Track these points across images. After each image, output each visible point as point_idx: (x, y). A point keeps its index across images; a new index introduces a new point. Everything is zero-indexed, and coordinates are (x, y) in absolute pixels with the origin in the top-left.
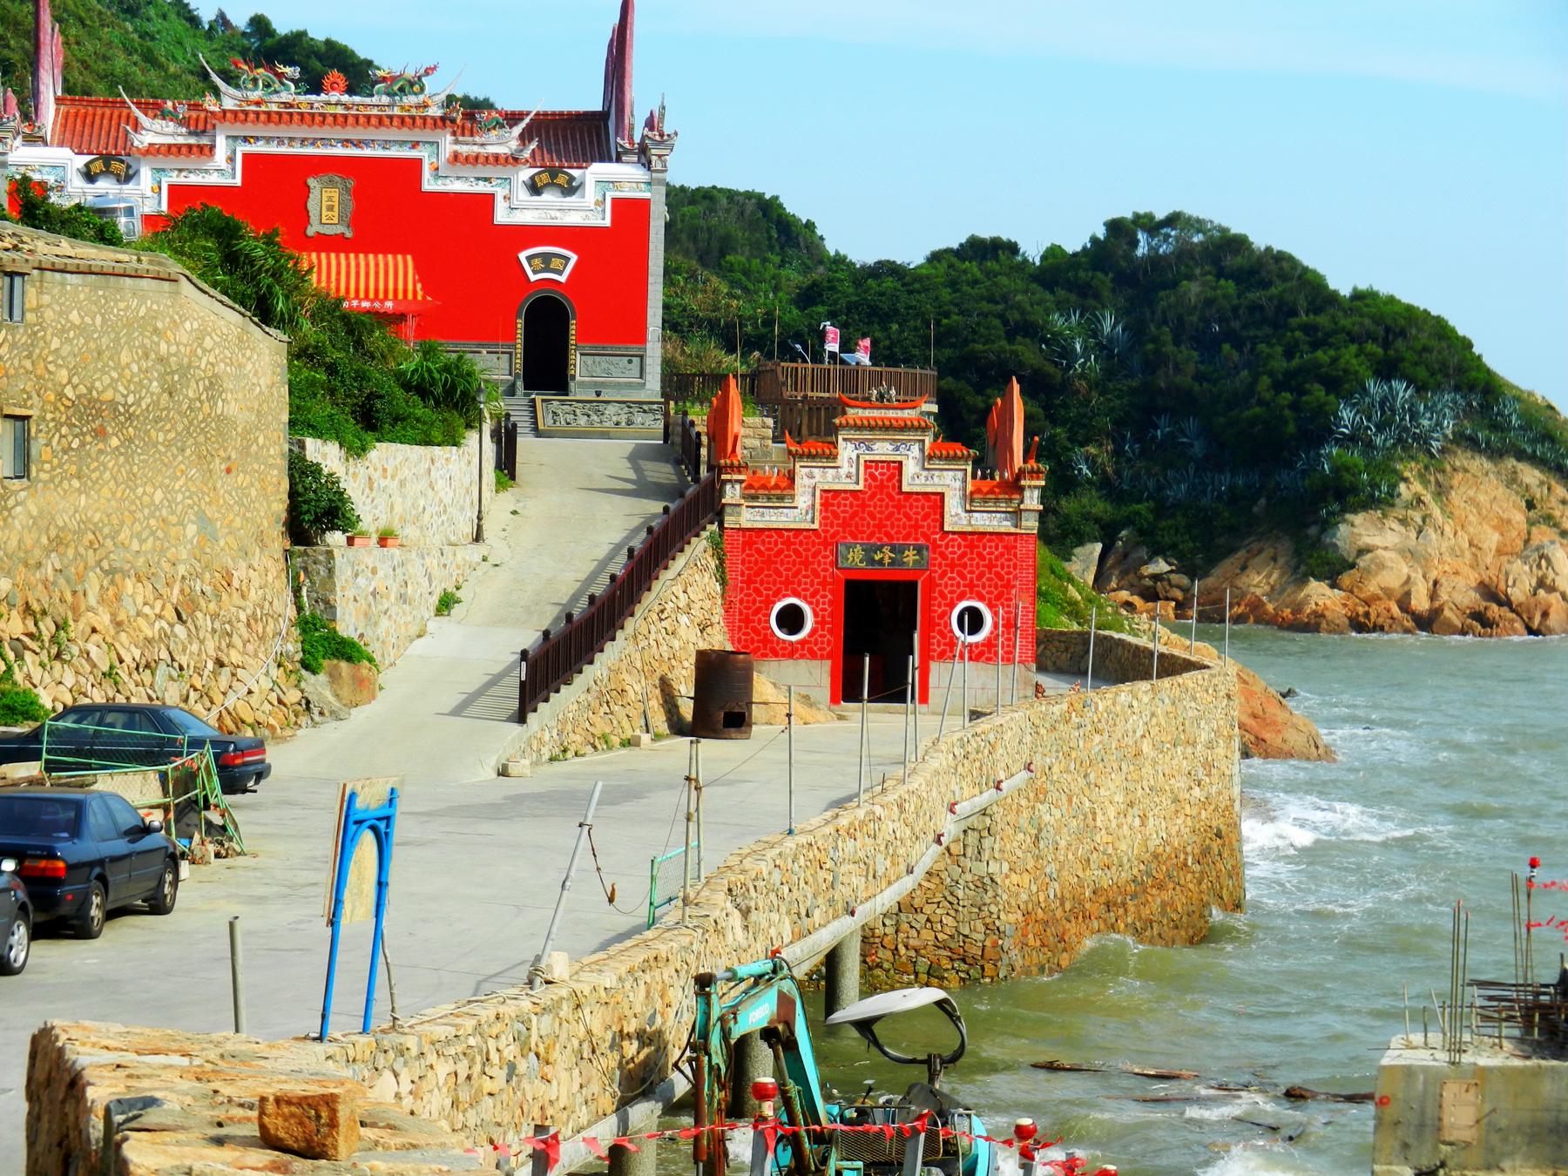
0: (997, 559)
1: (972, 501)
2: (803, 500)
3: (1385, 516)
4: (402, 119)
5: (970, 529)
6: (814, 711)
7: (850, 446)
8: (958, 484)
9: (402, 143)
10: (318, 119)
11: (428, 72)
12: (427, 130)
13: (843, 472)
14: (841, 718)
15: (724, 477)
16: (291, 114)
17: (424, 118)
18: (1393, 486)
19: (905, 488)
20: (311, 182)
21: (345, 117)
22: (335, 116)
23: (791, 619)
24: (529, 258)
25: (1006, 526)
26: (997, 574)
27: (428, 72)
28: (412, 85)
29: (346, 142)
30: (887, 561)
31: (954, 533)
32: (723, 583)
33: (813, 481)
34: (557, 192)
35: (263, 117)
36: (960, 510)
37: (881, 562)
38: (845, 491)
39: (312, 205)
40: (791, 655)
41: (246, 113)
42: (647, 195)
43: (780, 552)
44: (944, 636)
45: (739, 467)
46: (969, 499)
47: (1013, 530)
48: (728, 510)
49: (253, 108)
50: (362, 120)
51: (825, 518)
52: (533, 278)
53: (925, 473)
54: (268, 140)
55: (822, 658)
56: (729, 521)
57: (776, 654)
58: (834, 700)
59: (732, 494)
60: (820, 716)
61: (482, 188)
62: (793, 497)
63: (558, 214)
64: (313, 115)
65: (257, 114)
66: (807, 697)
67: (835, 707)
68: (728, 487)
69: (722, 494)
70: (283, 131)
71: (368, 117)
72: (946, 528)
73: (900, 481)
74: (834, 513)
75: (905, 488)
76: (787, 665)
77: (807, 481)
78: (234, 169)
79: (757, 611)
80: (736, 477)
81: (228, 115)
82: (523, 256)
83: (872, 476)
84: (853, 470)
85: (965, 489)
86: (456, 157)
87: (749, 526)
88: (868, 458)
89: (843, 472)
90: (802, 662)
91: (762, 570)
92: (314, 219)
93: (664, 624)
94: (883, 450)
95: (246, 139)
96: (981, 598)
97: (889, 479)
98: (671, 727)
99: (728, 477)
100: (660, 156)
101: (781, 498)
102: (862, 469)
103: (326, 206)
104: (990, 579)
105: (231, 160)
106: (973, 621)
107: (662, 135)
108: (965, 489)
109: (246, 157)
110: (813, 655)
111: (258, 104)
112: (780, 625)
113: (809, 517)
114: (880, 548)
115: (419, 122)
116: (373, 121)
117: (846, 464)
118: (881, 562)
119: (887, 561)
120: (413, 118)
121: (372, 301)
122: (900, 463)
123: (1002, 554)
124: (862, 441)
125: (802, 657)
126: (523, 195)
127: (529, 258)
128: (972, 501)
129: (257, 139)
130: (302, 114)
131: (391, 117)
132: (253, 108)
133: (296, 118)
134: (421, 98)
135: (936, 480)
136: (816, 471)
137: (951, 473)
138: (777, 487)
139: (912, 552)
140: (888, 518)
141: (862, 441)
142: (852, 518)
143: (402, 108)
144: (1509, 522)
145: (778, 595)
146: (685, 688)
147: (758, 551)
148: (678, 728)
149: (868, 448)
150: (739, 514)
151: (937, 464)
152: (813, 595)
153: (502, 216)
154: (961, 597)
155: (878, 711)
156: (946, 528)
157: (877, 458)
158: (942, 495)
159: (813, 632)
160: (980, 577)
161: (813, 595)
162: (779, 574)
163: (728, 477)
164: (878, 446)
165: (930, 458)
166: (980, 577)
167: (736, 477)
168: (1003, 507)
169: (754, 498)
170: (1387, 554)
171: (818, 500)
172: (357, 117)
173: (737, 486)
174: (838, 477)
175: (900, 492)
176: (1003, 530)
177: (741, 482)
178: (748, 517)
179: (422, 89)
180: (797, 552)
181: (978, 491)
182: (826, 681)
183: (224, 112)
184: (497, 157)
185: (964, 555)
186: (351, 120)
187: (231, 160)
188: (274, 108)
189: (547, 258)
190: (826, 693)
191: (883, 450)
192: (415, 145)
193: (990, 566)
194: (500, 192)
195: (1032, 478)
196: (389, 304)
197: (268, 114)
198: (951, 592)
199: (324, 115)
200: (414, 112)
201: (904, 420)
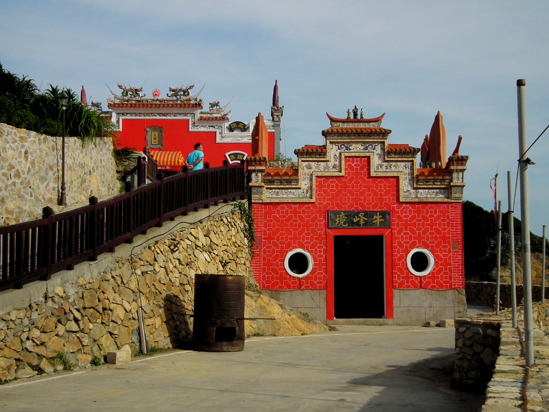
0: (436, 220)
1: (418, 181)
2: (304, 184)
3: (505, 268)
4: (181, 105)
5: (417, 200)
6: (311, 325)
7: (335, 147)
8: (408, 171)
9: (180, 114)
10: (149, 105)
11: (191, 88)
12: (190, 108)
13: (330, 164)
14: (332, 329)
15: (250, 168)
16: (139, 104)
17: (189, 104)
18: (507, 260)
19: (373, 174)
20: (148, 129)
21: (160, 105)
22: (156, 105)
23: (299, 263)
24: (229, 155)
25: (441, 197)
26: (436, 230)
27: (191, 88)
28: (186, 92)
29: (159, 114)
30: (362, 222)
31: (406, 203)
32: (251, 239)
33: (311, 171)
34: (239, 130)
35: (129, 105)
36: (409, 188)
37: (358, 223)
38: (333, 177)
39: (148, 137)
40: (299, 287)
41: (123, 104)
42: (273, 130)
43: (290, 218)
44: (402, 272)
45: (260, 160)
46: (417, 180)
47: (446, 200)
48: (254, 190)
49: (126, 102)
50: (166, 105)
51: (319, 195)
52: (231, 162)
53: (385, 164)
54: (131, 114)
55: (320, 289)
56: (255, 198)
57: (289, 287)
58: (329, 317)
59: (256, 180)
60: (316, 329)
61: (211, 130)
62: (297, 181)
63: (240, 139)
64: (148, 104)
65: (127, 104)
66: (306, 315)
67: (329, 322)
68: (253, 175)
69: (249, 180)
70: (137, 111)
71: (168, 105)
72: (401, 200)
73: (369, 170)
74: (325, 191)
75: (373, 174)
76: (297, 293)
77: (306, 171)
78: (119, 125)
79: (276, 257)
80: (258, 168)
81: (117, 105)
82: (227, 155)
83: (350, 166)
84: (337, 163)
85: (412, 174)
86: (201, 118)
87: (268, 201)
88: (347, 154)
89: (330, 164)
90: (307, 291)
91: (278, 230)
92: (149, 143)
93: (176, 255)
94: (357, 149)
95: (123, 114)
96: (426, 247)
97: (362, 169)
98: (172, 341)
99: (253, 168)
100: (277, 116)
101: (289, 182)
102: (343, 162)
103: (152, 137)
104: (432, 234)
105: (118, 122)
106: (420, 262)
107: (278, 107)
108: (412, 174)
109: (123, 120)
110: (314, 288)
111: (127, 101)
112: (292, 268)
113: (308, 195)
114: (357, 214)
115: (187, 106)
116: (170, 106)
117: (332, 160)
118: (358, 223)
119: (362, 222)
120: (185, 104)
121: (162, 167)
122: (369, 157)
123: (439, 217)
124: (343, 143)
125: (307, 288)
126: (226, 132)
127: (229, 155)
128: (418, 181)
129: (127, 114)
130: (144, 104)
131: (176, 104)
132: (126, 102)
133: (141, 105)
134: (188, 97)
135: (393, 168)
136: (312, 164)
137: (403, 164)
138: (286, 174)
139: (378, 217)
140: (362, 194)
141: (343, 143)
142: (337, 195)
143: (181, 101)
144: (538, 269)
145: (289, 247)
146: (188, 301)
147: (275, 218)
148: (181, 341)
149: (347, 148)
150: (261, 193)
151: (394, 158)
152: (313, 246)
153: (219, 140)
154: (412, 247)
155: (359, 324)
156: (401, 200)
157: (353, 154)
158: (397, 178)
159: (314, 270)
160: (424, 233)
161: (313, 246)
162: (289, 233)
163: (253, 168)
164: (353, 147)
165: (389, 153)
166: (424, 233)
167: (258, 168)
168: (438, 185)
169: (272, 182)
170: (506, 278)
171: (314, 183)
172: (164, 105)
173: (260, 174)
174: (327, 167)
175: (369, 177)
176: (439, 200)
177: (262, 171)
178: (268, 195)
179: (188, 94)
180: (301, 218)
181: (422, 174)
182: (323, 304)
183: (115, 104)
184: (216, 118)
185: (414, 217)
186: (162, 105)
187: (118, 122)
188: (134, 102)
189: (236, 155)
190: (323, 312)
191: (357, 149)
192: (186, 115)
193: (432, 225)
194: (218, 131)
195: (458, 164)
196: (168, 168)
197: (131, 104)
198: (405, 243)
199: (151, 104)
200: (185, 102)
201: (371, 129)
